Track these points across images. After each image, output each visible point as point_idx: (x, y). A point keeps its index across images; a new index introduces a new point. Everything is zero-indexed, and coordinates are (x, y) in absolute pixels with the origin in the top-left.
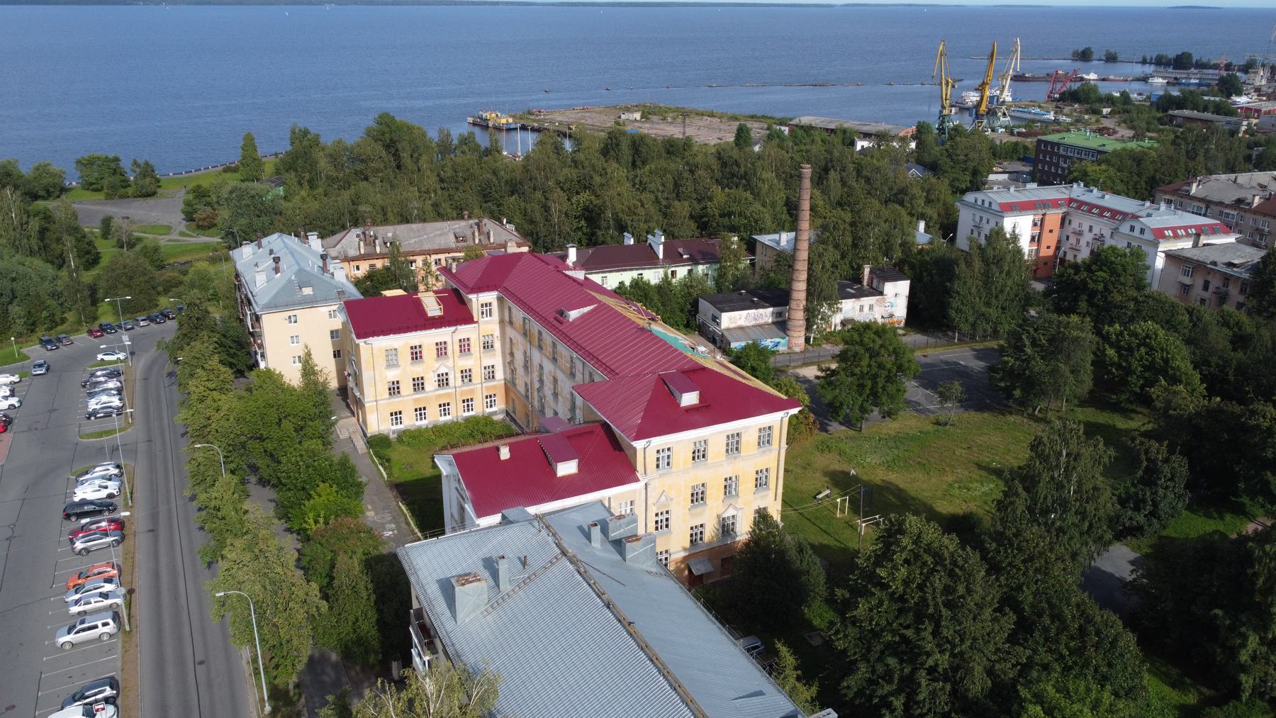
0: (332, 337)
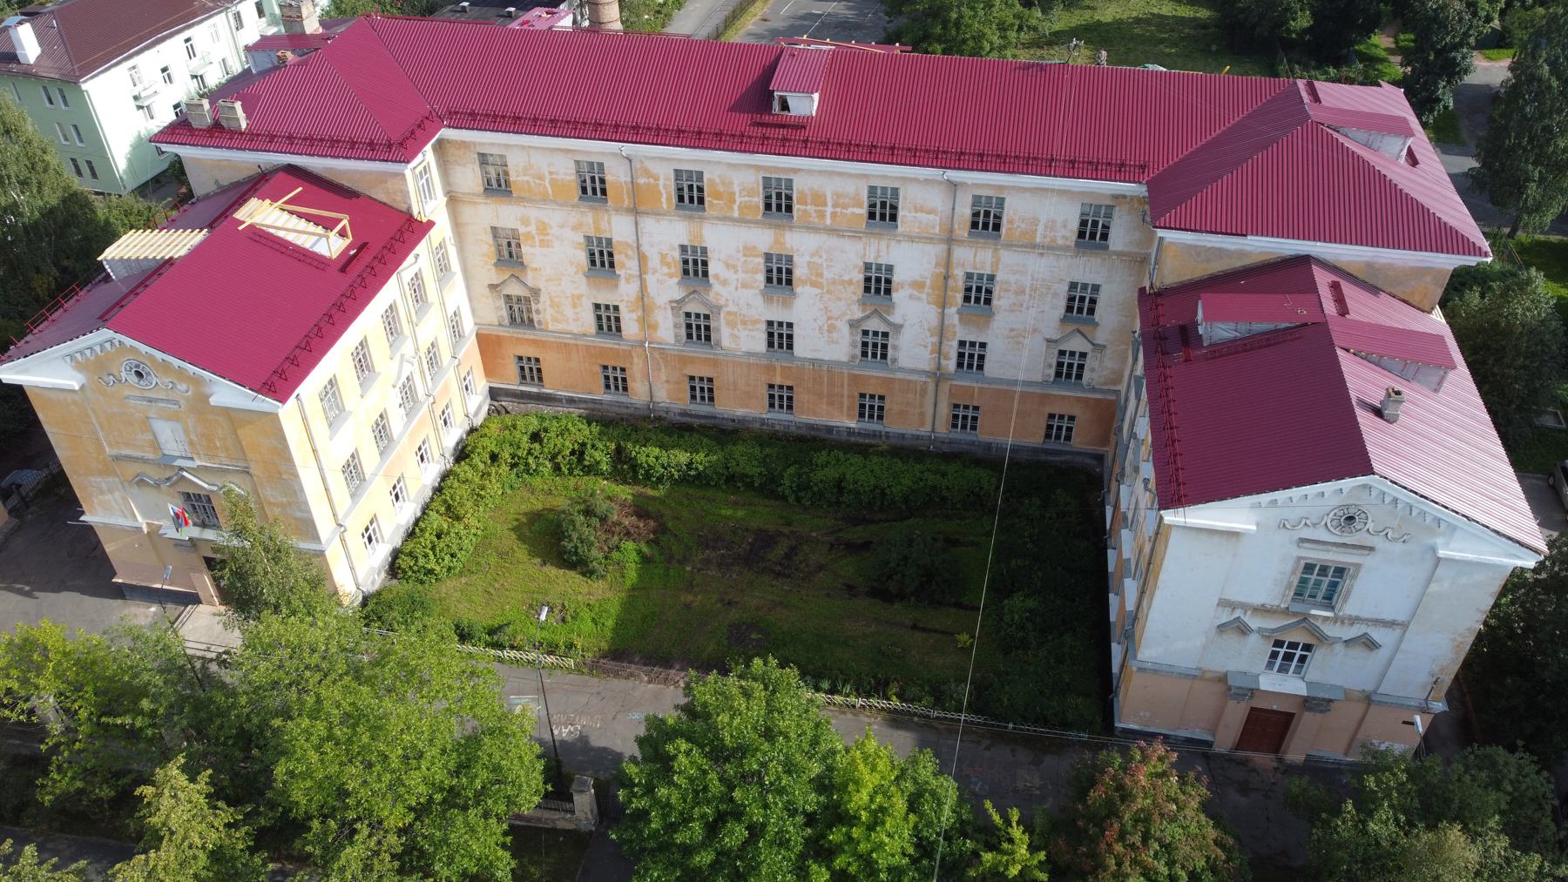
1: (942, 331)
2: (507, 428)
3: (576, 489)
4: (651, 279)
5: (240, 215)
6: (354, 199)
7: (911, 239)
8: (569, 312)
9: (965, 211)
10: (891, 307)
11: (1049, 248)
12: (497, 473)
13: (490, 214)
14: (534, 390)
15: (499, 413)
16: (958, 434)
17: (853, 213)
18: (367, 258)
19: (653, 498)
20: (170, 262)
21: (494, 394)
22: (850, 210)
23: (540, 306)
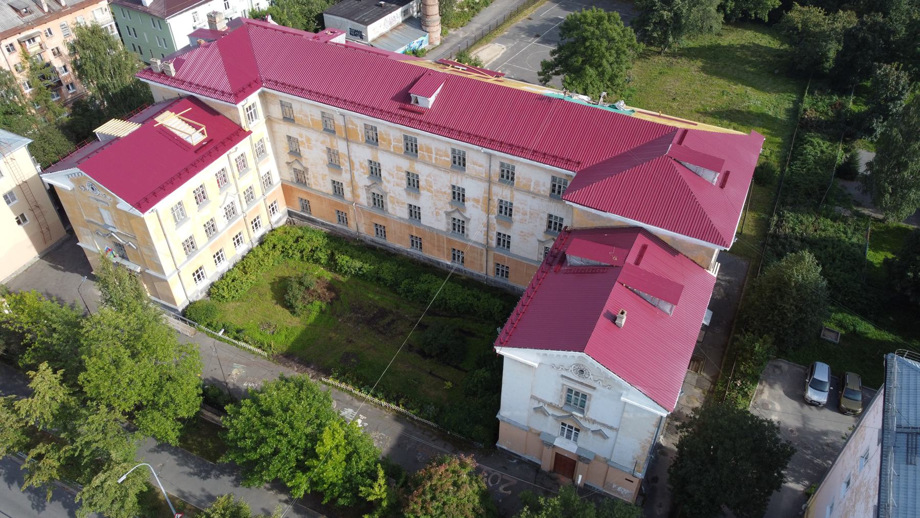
0: (8, 203)
1: (488, 226)
2: (286, 233)
3: (307, 269)
4: (356, 174)
5: (157, 119)
6: (216, 116)
7: (473, 178)
8: (321, 182)
9: (496, 169)
10: (464, 209)
11: (535, 195)
12: (273, 254)
13: (284, 129)
14: (307, 215)
15: (291, 223)
16: (499, 279)
17: (445, 160)
18: (211, 147)
19: (341, 282)
20: (118, 138)
21: (290, 213)
22: (443, 158)
23: (309, 176)
